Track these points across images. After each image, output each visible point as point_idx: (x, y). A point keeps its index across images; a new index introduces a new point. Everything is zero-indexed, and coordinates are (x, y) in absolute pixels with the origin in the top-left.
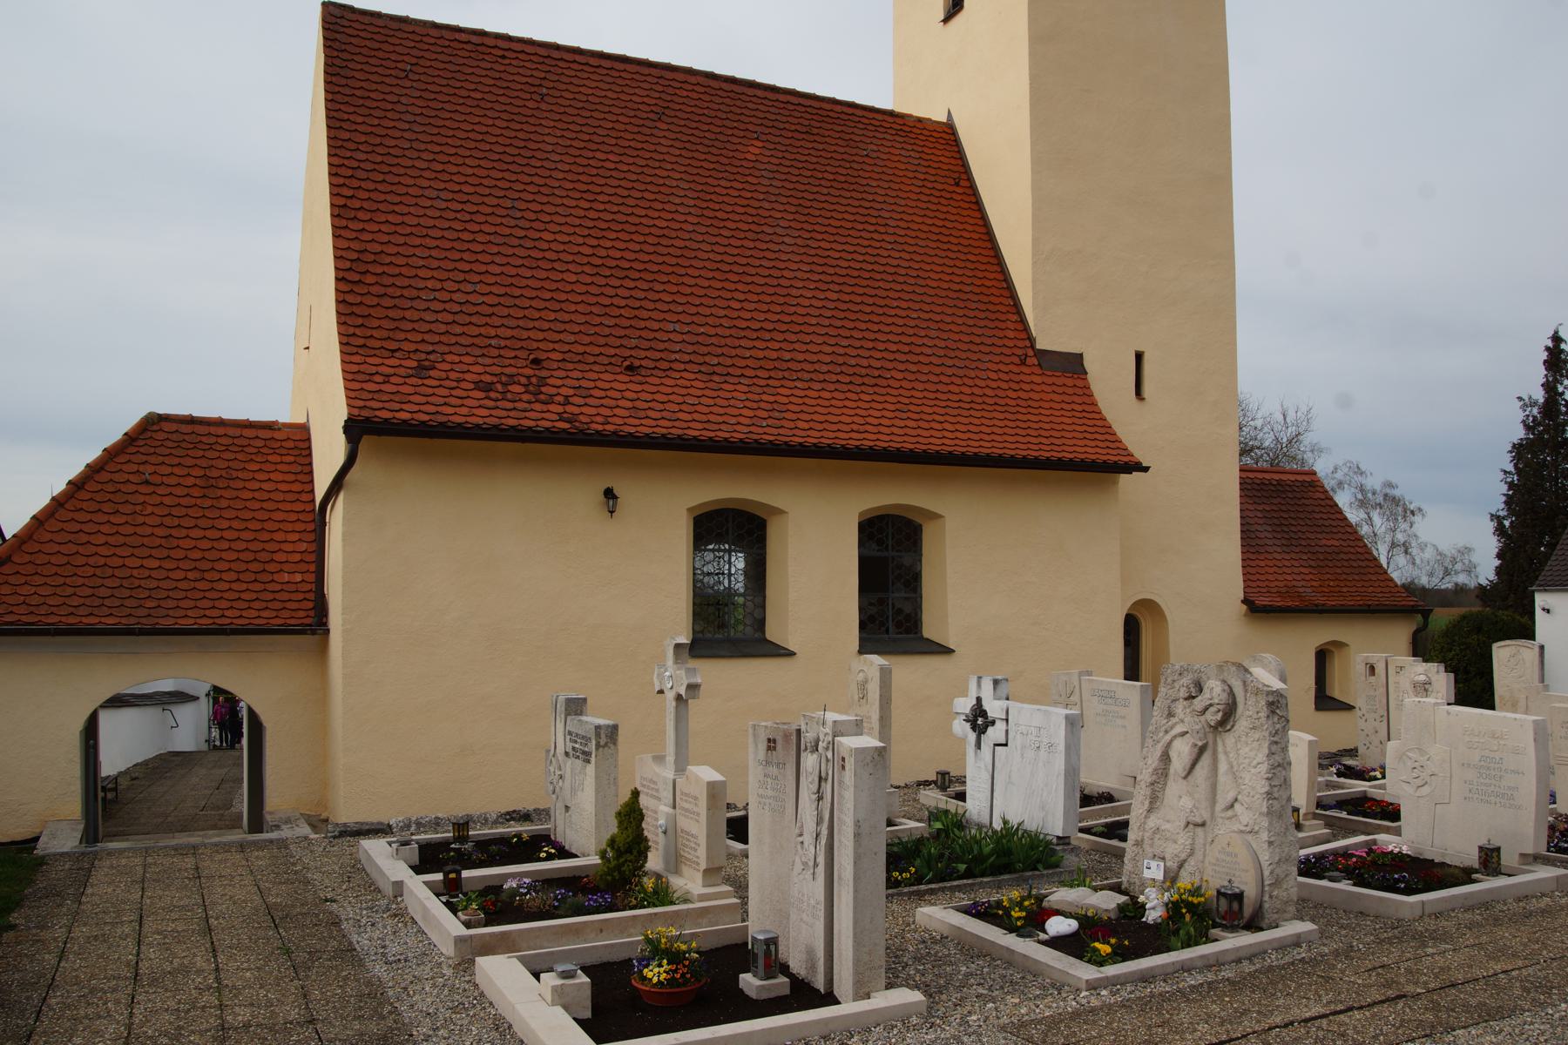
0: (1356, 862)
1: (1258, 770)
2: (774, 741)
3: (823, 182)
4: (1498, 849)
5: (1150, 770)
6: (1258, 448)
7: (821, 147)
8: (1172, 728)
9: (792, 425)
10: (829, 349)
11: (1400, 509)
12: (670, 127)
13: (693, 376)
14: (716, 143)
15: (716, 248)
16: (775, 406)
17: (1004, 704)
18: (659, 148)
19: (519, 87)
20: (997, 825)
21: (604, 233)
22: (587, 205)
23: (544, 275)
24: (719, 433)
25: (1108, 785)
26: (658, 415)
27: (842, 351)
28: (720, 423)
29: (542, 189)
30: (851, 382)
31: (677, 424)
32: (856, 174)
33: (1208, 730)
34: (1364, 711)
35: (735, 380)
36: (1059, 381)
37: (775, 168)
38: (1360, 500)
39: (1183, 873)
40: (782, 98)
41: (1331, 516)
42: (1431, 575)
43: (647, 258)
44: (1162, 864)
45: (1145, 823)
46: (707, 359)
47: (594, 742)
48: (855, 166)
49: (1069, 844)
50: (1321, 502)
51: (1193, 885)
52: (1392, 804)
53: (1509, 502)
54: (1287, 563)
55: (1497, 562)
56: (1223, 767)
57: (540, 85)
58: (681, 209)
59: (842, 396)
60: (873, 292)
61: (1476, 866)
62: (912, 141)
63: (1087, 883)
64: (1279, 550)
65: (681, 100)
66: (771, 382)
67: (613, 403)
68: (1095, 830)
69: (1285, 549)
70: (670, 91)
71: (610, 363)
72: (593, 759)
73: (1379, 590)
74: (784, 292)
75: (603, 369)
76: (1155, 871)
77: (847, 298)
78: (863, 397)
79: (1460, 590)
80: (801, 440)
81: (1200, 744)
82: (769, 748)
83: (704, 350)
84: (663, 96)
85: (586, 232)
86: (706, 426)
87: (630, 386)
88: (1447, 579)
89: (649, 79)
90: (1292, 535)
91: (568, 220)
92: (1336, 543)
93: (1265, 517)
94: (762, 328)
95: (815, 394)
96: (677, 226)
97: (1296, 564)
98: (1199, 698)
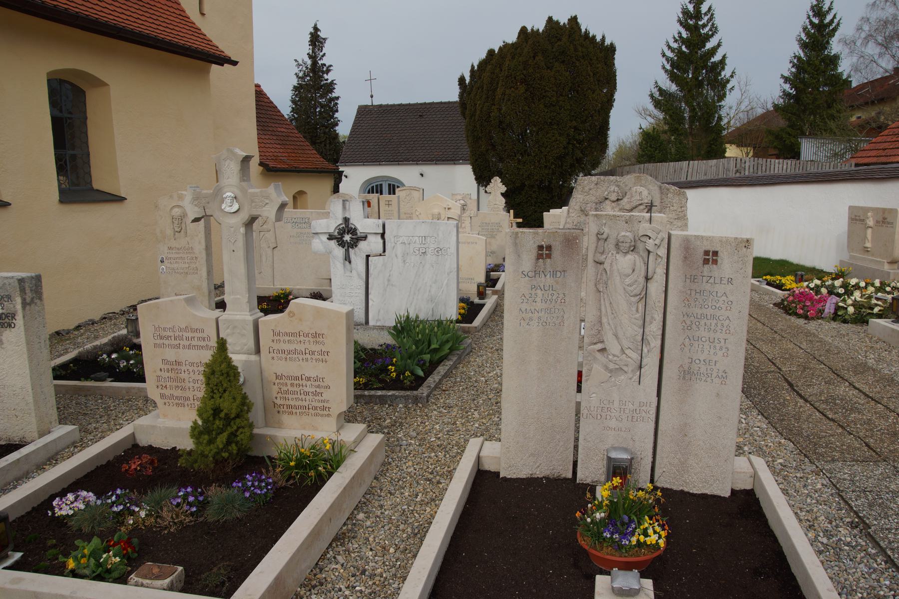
2: (549, 248)
47: (19, 300)
82: (539, 257)
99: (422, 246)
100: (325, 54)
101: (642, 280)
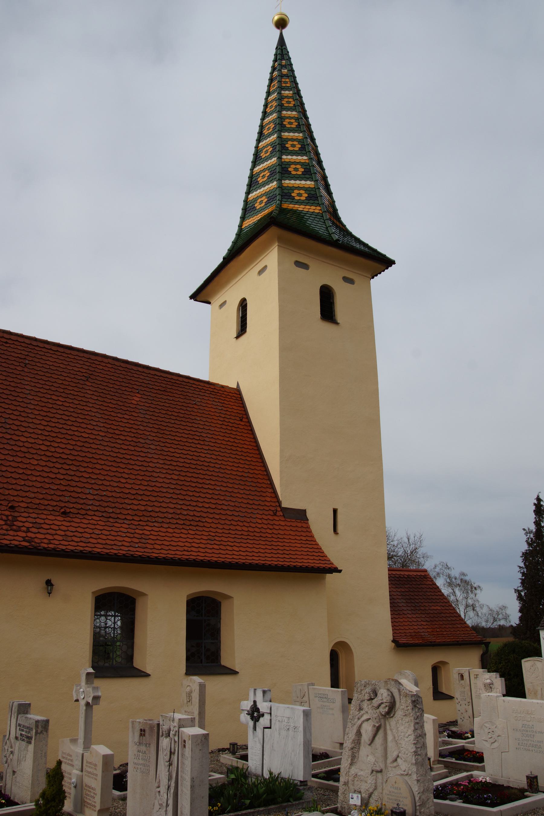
0: (463, 789)
1: (409, 739)
2: (144, 731)
3: (172, 417)
4: (536, 777)
5: (351, 741)
6: (395, 556)
7: (171, 398)
8: (362, 716)
9: (151, 547)
10: (172, 506)
11: (469, 587)
12: (93, 385)
13: (98, 519)
14: (116, 394)
15: (114, 449)
16: (143, 536)
17: (268, 704)
18: (86, 395)
19: (14, 359)
20: (266, 775)
21: (54, 439)
22: (45, 423)
23: (20, 460)
24: (111, 551)
25: (326, 748)
26: (79, 540)
27: (179, 507)
28: (112, 545)
29: (22, 414)
30: (184, 524)
31: (88, 545)
32: (189, 413)
33: (381, 717)
34: (459, 700)
35: (122, 521)
36: (294, 524)
37: (147, 409)
38: (449, 583)
39: (371, 800)
40: (152, 372)
41: (436, 594)
42: (487, 621)
43: (76, 453)
44: (360, 796)
45: (349, 772)
46: (107, 509)
47: (34, 731)
48: (189, 409)
49: (307, 785)
50: (430, 586)
51: (377, 807)
52: (478, 752)
53: (523, 582)
54: (415, 620)
55: (520, 614)
56: (390, 738)
57: (25, 359)
58: (96, 428)
59: (179, 531)
60: (197, 476)
61: (526, 787)
62: (219, 397)
63: (319, 808)
64: (410, 612)
65: (99, 371)
66: (141, 523)
67: (54, 532)
68: (320, 775)
69: (413, 612)
70: (94, 365)
71: (53, 510)
72: (33, 741)
73: (462, 632)
74: (149, 474)
75: (49, 513)
76: (355, 800)
77: (183, 478)
78: (190, 532)
79: (501, 628)
80: (157, 555)
81: (377, 725)
83: (106, 504)
84: (90, 368)
85: (44, 438)
86: (105, 546)
87: (64, 523)
88: (495, 623)
89: (83, 359)
90: (417, 604)
91: (35, 431)
92: (439, 608)
93: (402, 595)
94: (137, 493)
95: (164, 530)
96: (94, 437)
97: (419, 620)
98: (376, 699)
99: (288, 724)
101: (169, 753)
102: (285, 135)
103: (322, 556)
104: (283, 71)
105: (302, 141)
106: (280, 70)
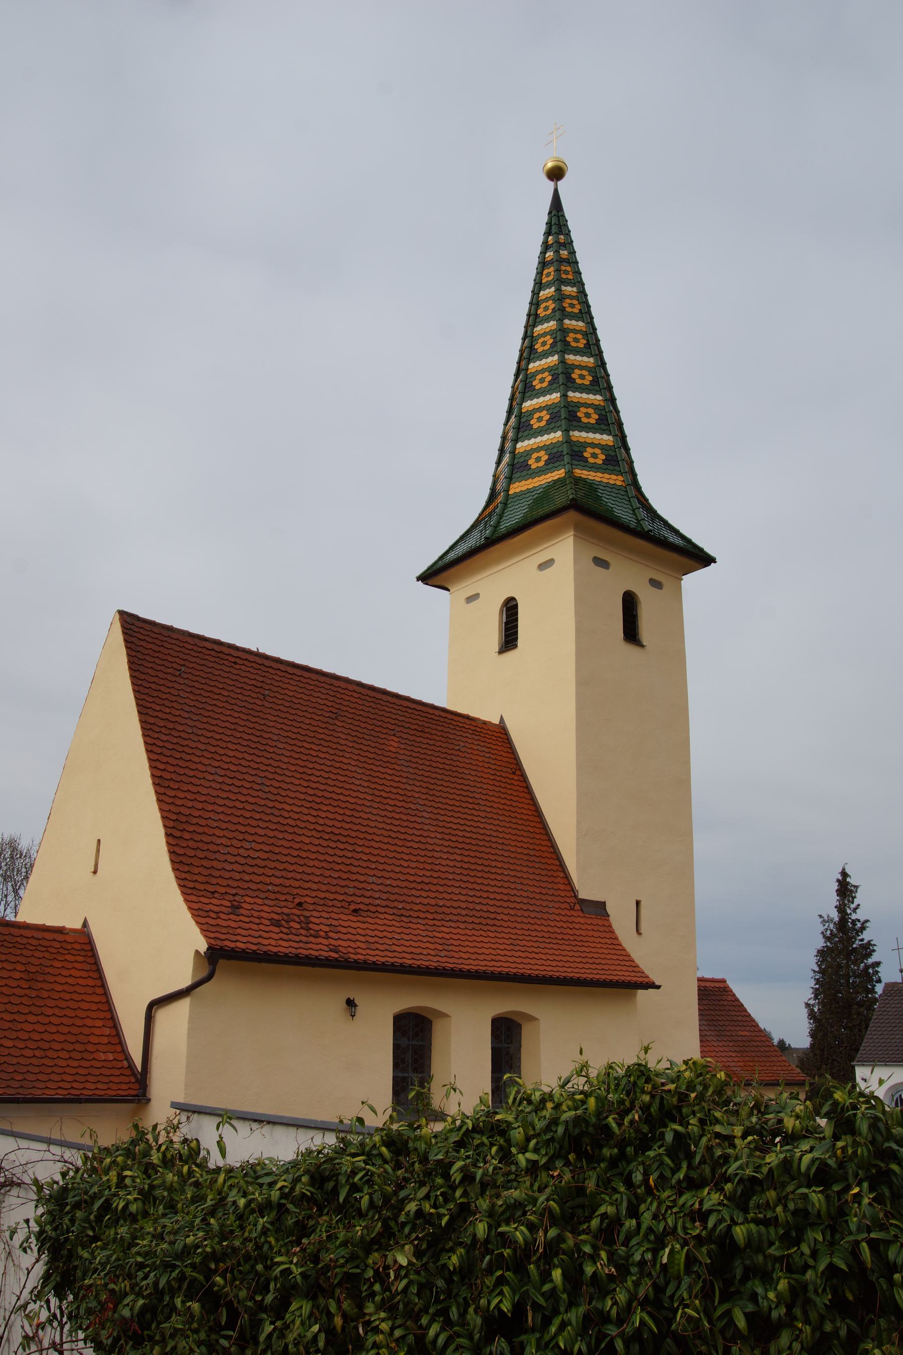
36: (595, 922)
92: (748, 1034)
100: (859, 905)
102: (570, 358)
103: (634, 967)
104: (561, 252)
105: (593, 370)
106: (557, 252)
